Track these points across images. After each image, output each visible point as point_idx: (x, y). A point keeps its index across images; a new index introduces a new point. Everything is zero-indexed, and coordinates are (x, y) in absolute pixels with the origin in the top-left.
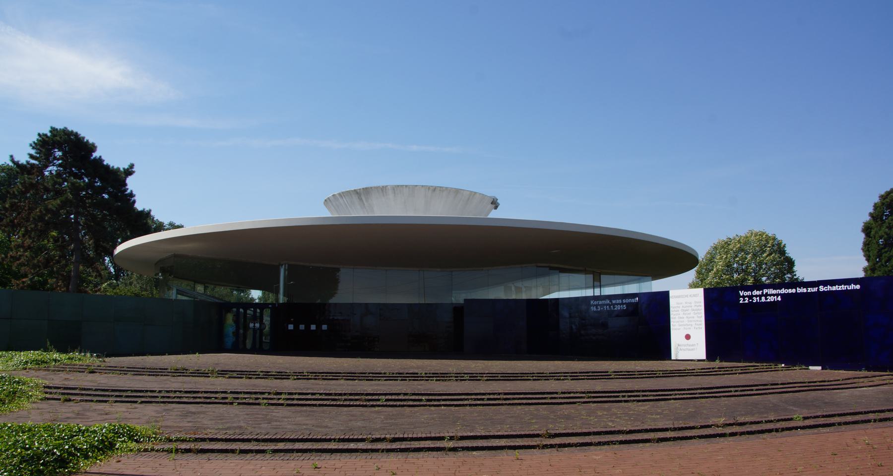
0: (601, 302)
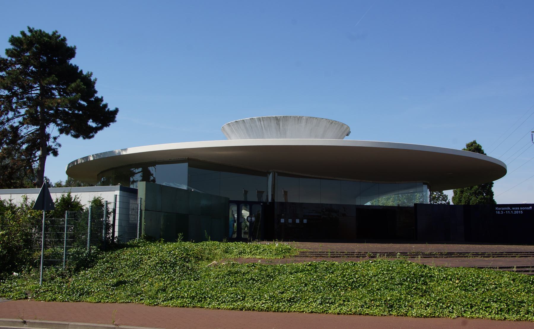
0: (503, 209)
